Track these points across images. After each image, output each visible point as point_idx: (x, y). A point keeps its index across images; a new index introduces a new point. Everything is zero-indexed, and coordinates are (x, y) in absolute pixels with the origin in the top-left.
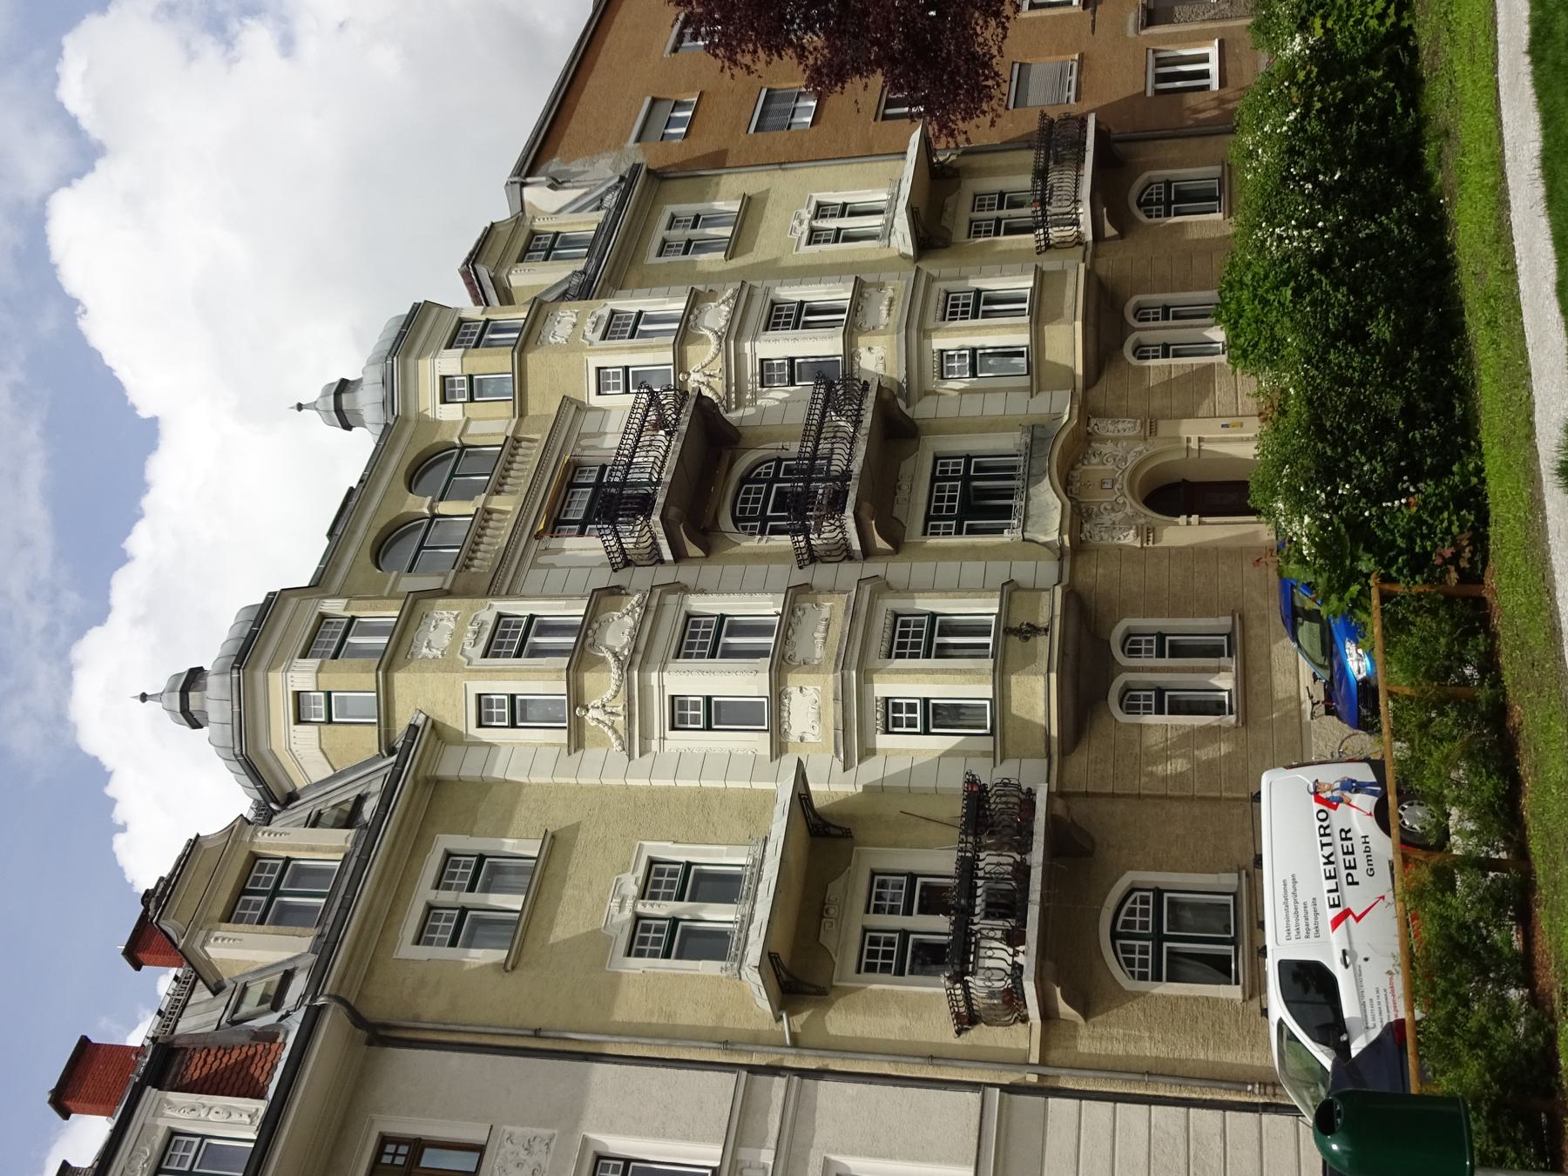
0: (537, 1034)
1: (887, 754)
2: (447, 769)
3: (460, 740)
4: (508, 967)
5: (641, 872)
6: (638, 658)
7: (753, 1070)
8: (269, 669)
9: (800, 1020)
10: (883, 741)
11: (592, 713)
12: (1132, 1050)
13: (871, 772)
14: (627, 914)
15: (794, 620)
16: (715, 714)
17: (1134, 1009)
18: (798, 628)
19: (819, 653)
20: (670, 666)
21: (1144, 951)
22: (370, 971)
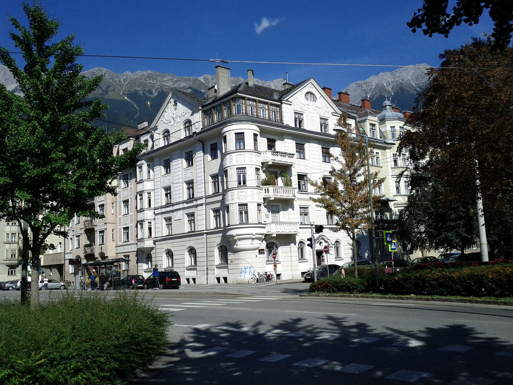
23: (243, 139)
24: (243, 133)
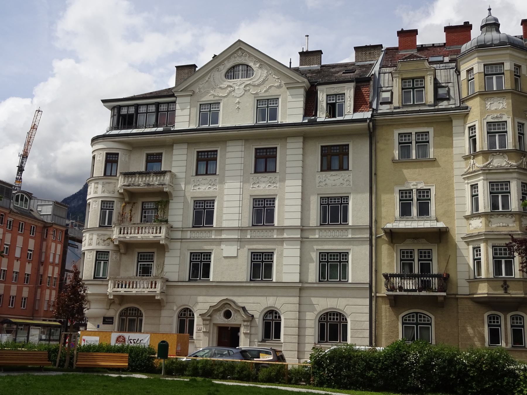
0: (375, 174)
1: (468, 249)
2: (455, 123)
3: (465, 123)
4: (394, 161)
5: (425, 188)
6: (486, 171)
7: (371, 228)
8: (478, 57)
9: (385, 237)
10: (471, 247)
11: (472, 161)
12: (383, 317)
13: (461, 245)
14: (412, 187)
15: (507, 216)
16: (475, 197)
17: (394, 318)
18: (504, 217)
19: (494, 226)
20: (486, 182)
21: (413, 320)
22: (390, 125)
23: (116, 162)
24: (118, 154)
